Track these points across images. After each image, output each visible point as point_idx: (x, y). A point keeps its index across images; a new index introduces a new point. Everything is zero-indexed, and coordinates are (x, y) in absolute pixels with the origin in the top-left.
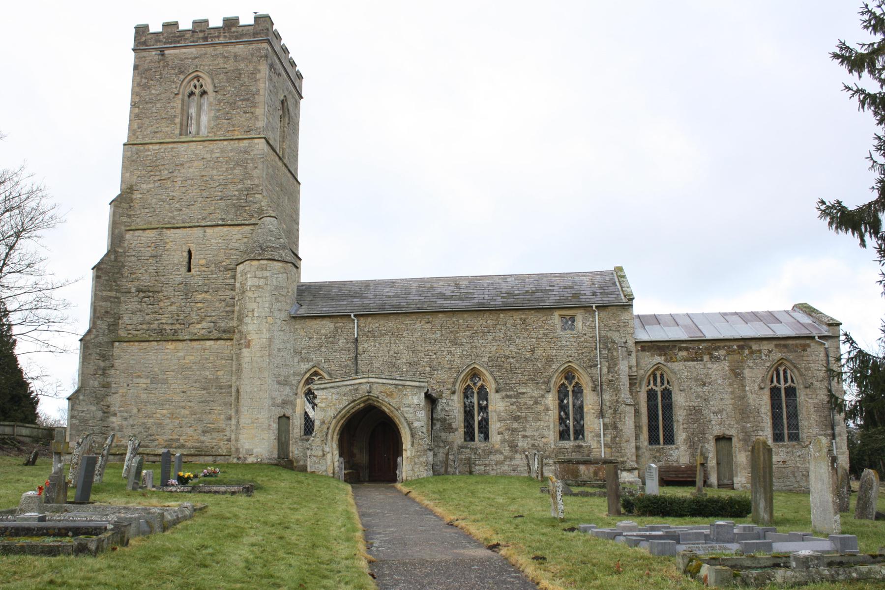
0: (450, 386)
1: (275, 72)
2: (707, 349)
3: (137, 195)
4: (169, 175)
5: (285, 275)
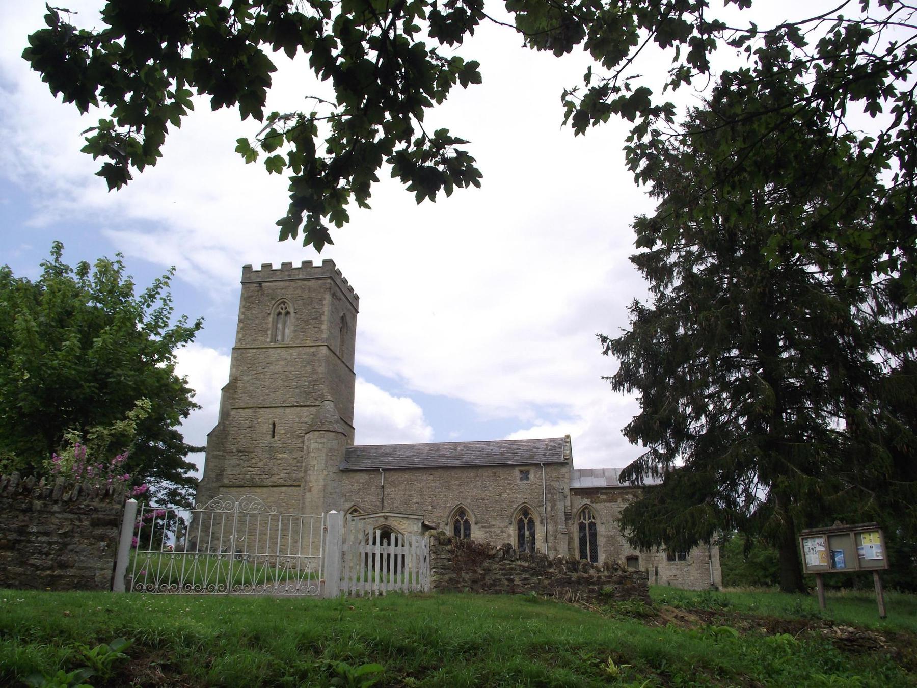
0: (444, 520)
1: (337, 298)
2: (620, 493)
3: (240, 384)
4: (263, 370)
5: (336, 442)
